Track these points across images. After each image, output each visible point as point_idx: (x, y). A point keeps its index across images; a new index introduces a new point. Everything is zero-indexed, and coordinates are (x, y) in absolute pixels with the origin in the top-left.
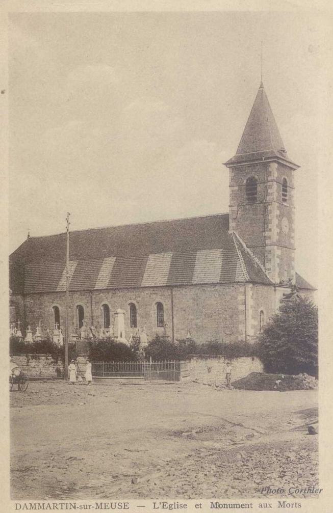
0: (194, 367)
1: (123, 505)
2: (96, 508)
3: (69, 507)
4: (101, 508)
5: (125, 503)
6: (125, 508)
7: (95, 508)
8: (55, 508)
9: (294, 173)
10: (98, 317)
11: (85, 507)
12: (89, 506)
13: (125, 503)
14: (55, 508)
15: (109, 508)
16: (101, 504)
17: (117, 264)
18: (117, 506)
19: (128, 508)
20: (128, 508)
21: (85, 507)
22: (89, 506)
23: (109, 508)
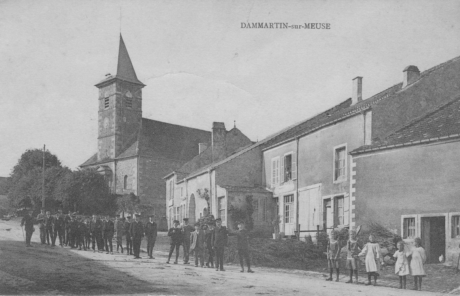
0: (197, 177)
1: (325, 26)
2: (305, 28)
3: (282, 27)
4: (256, 27)
5: (327, 24)
6: (327, 28)
7: (305, 27)
8: (271, 27)
9: (143, 89)
10: (379, 259)
11: (296, 27)
12: (300, 26)
13: (327, 24)
14: (271, 27)
15: (314, 28)
16: (256, 24)
17: (457, 218)
18: (321, 26)
19: (330, 28)
20: (330, 28)
21: (296, 27)
22: (300, 26)
23: (314, 28)
